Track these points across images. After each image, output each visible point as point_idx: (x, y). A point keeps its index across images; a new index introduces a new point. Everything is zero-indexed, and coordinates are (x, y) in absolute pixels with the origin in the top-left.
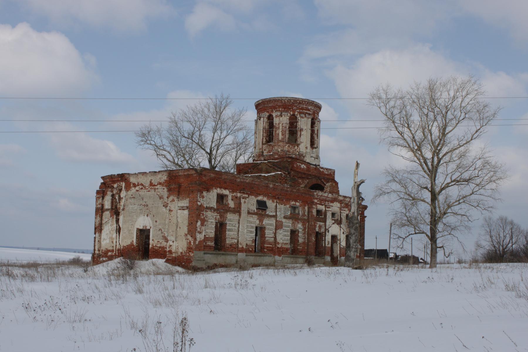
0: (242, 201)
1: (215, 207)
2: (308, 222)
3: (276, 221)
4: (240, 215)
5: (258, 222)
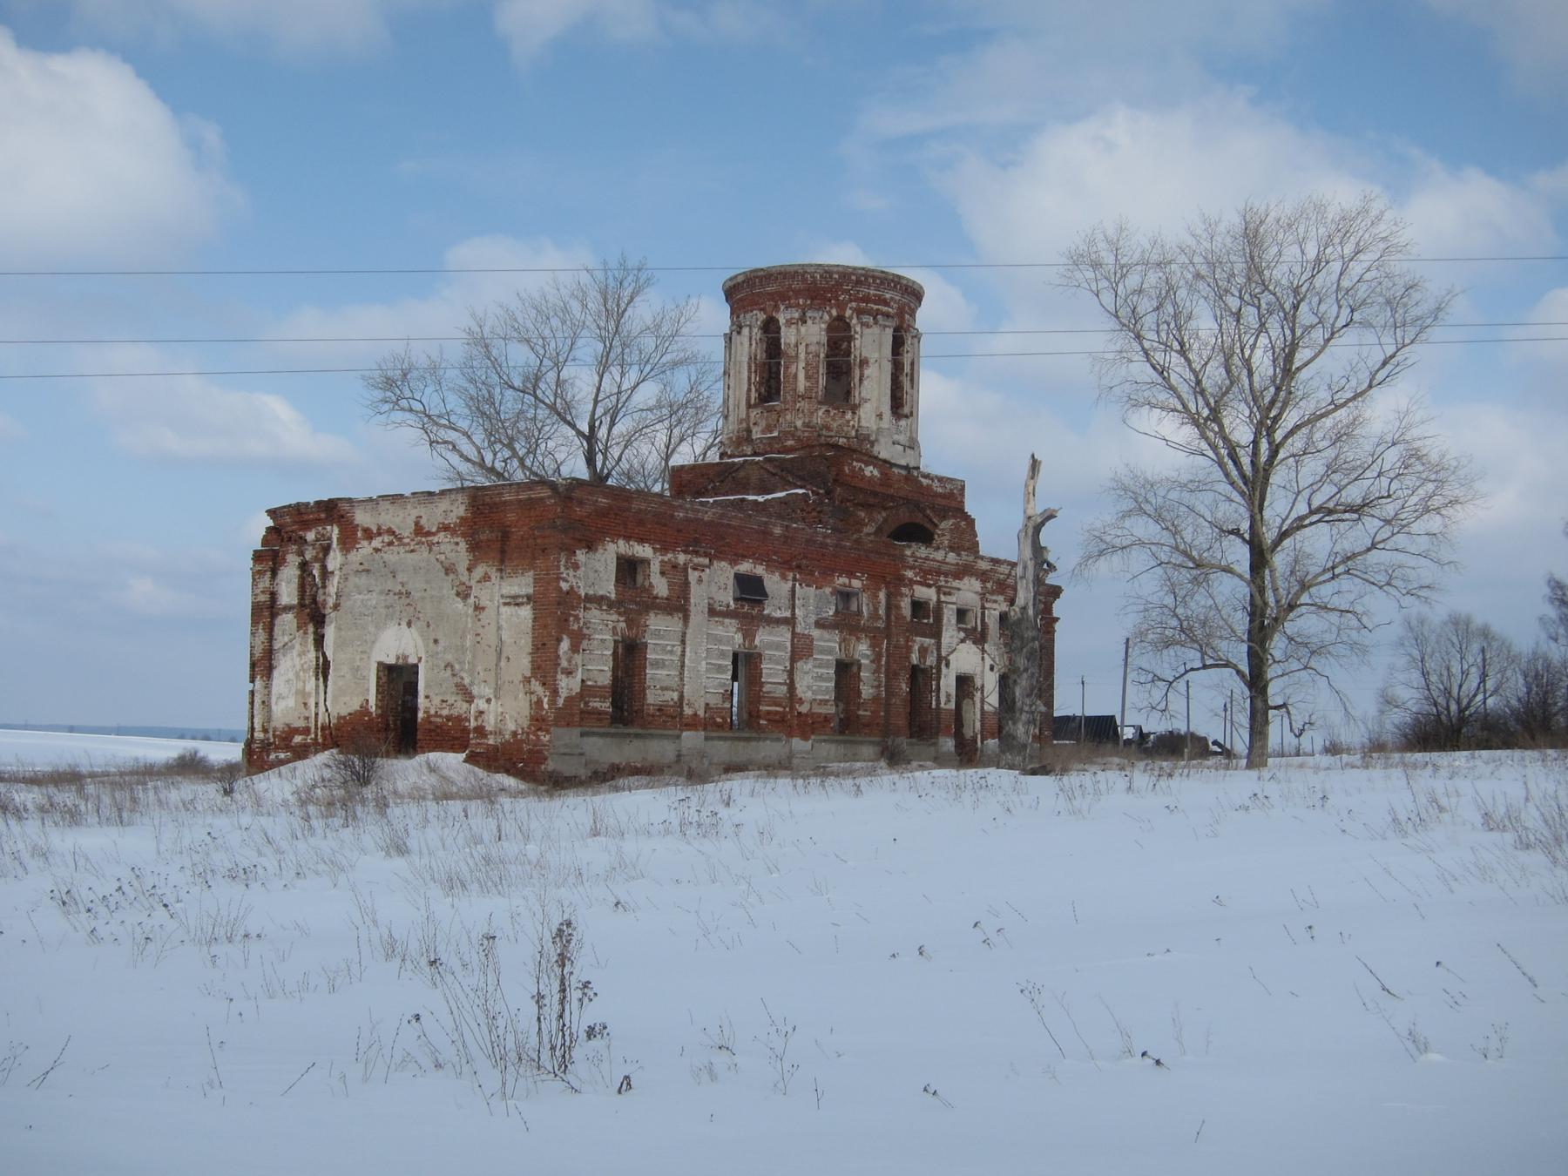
0: (693, 576)
1: (613, 596)
2: (888, 637)
4: (686, 619)
5: (739, 638)
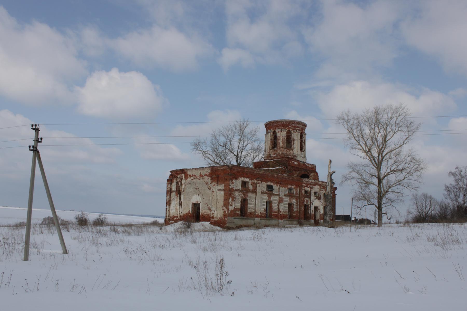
0: (258, 185)
2: (300, 198)
3: (279, 198)
4: (256, 194)
5: (267, 198)
